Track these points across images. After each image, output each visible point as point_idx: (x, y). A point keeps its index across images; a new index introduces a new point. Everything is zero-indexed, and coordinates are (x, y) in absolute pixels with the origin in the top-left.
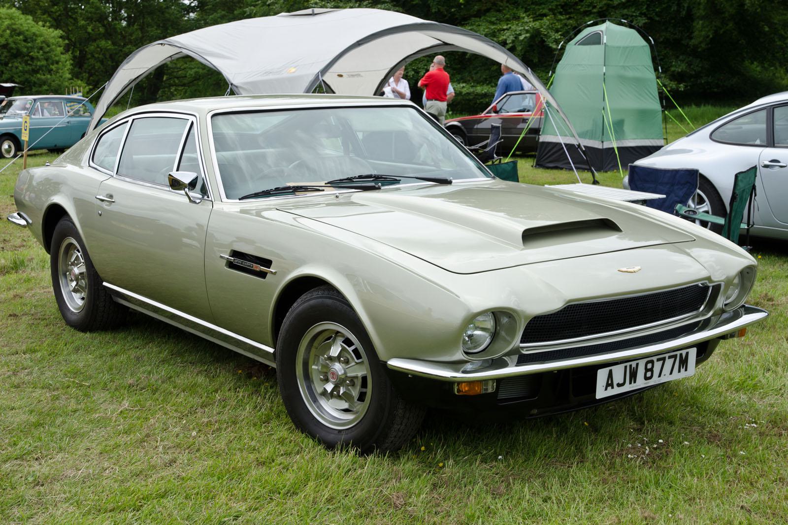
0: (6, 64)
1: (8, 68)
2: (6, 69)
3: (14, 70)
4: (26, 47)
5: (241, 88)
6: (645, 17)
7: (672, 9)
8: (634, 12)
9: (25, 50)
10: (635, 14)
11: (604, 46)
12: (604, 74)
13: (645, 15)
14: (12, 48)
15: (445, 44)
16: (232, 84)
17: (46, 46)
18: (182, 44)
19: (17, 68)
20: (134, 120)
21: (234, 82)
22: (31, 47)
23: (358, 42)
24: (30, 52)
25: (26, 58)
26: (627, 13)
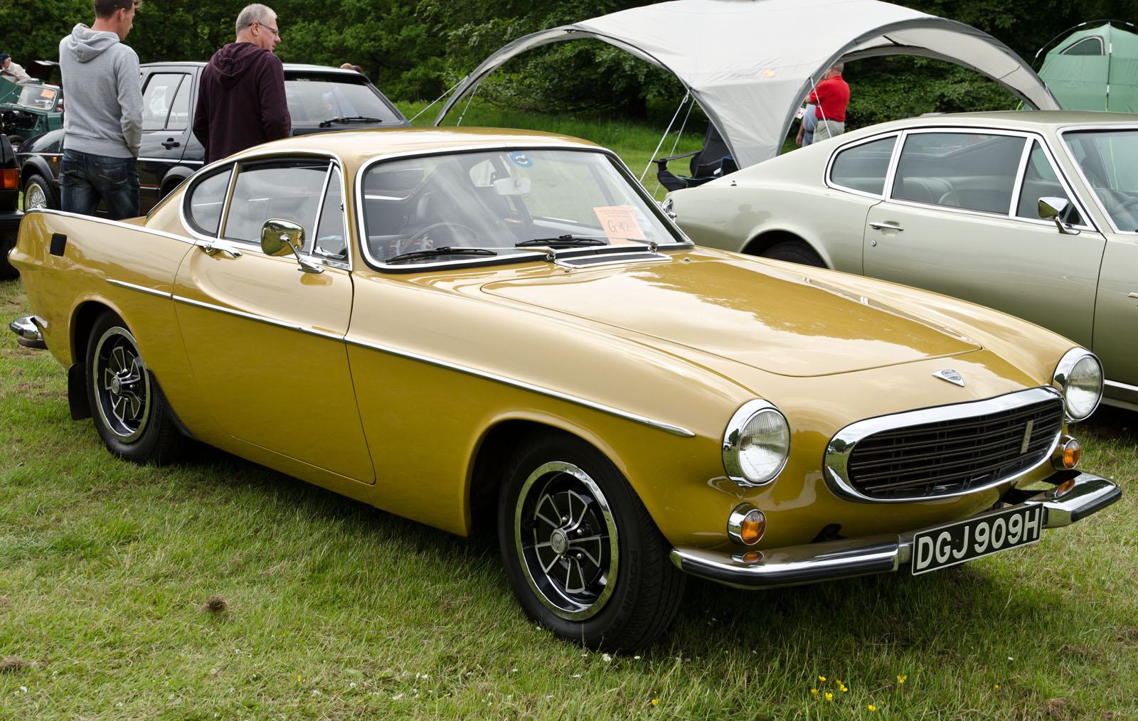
0: (28, 32)
1: (30, 37)
2: (28, 39)
3: (39, 40)
4: (58, 8)
5: (703, 93)
6: (1011, 14)
7: (1050, 5)
8: (996, 6)
9: (56, 13)
10: (998, 10)
11: (1107, 57)
12: (1108, 95)
13: (1011, 11)
14: (38, 9)
15: (896, 45)
16: (691, 88)
17: (86, 8)
18: (598, 30)
19: (44, 37)
20: (908, 135)
21: (694, 86)
22: (65, 8)
23: (855, 40)
24: (63, 17)
25: (57, 24)
26: (987, 7)
